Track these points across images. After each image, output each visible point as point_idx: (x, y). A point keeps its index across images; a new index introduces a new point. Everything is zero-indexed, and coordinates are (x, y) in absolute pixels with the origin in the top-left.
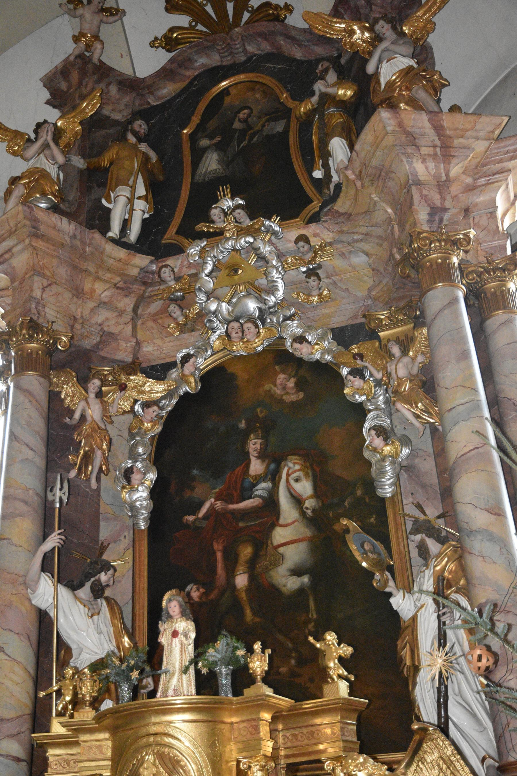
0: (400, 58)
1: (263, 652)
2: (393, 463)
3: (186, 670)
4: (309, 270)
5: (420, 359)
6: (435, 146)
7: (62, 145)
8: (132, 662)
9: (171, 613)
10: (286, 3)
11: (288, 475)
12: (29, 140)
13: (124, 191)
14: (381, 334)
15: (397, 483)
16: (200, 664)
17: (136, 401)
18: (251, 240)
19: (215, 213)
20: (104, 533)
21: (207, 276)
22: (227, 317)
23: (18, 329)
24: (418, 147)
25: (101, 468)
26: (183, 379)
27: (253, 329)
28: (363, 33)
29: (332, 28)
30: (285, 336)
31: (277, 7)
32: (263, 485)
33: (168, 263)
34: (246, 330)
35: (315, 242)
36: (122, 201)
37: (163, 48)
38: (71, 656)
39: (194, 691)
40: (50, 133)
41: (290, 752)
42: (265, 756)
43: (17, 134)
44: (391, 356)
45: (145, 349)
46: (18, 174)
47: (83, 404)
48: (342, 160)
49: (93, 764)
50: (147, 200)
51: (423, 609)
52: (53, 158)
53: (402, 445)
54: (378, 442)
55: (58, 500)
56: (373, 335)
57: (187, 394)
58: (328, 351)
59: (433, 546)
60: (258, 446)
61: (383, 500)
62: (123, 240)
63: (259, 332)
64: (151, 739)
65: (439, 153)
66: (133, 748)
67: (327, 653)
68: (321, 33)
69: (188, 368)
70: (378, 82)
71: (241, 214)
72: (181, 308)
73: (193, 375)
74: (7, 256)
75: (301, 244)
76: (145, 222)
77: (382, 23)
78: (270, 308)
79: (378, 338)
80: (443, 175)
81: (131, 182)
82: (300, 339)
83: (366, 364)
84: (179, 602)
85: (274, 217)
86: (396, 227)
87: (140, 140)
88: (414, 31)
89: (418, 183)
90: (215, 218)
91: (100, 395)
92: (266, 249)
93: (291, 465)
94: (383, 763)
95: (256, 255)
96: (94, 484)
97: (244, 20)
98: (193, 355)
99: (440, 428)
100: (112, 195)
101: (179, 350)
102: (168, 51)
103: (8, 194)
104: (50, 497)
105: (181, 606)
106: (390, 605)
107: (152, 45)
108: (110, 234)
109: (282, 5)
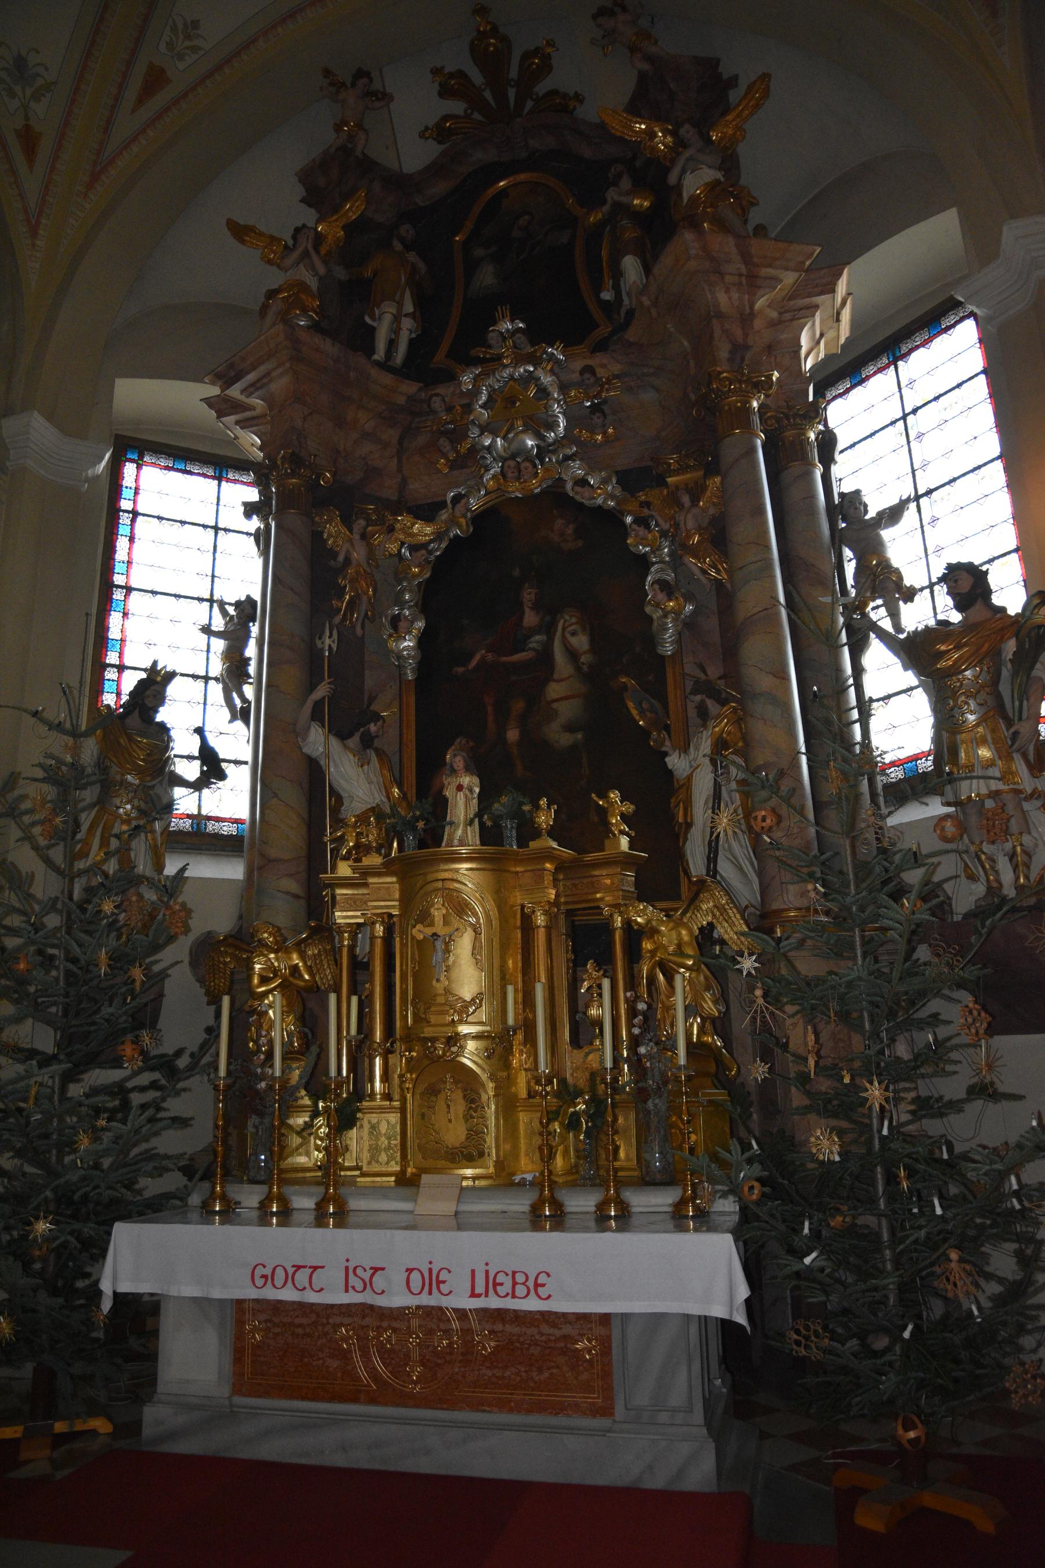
0: (706, 169)
1: (549, 807)
2: (674, 620)
3: (471, 823)
4: (593, 404)
5: (712, 511)
6: (741, 275)
7: (323, 252)
8: (418, 813)
9: (456, 767)
10: (576, 92)
11: (564, 629)
12: (286, 247)
13: (389, 310)
14: (669, 480)
15: (679, 641)
16: (486, 817)
17: (403, 544)
18: (532, 369)
19: (492, 337)
20: (370, 681)
21: (481, 407)
22: (503, 454)
23: (279, 463)
24: (722, 275)
25: (366, 614)
26: (453, 521)
27: (531, 469)
28: (664, 136)
29: (631, 129)
30: (564, 476)
31: (565, 96)
32: (538, 638)
33: (437, 391)
34: (522, 468)
35: (601, 372)
36: (388, 318)
37: (434, 139)
38: (342, 804)
39: (478, 842)
40: (310, 240)
41: (569, 899)
42: (549, 902)
43: (273, 239)
44: (681, 506)
45: (411, 487)
46: (275, 286)
47: (347, 546)
48: (634, 282)
49: (383, 903)
50: (414, 318)
51: (699, 770)
52: (313, 268)
53: (686, 601)
54: (661, 596)
55: (327, 648)
56: (661, 482)
57: (456, 536)
58: (612, 497)
59: (712, 706)
60: (533, 596)
61: (662, 658)
62: (389, 363)
63: (537, 473)
64: (440, 884)
65: (744, 282)
66: (422, 892)
67: (610, 809)
68: (618, 134)
69: (460, 508)
70: (680, 195)
71: (521, 339)
72: (451, 442)
73: (464, 516)
74: (265, 380)
75: (587, 376)
76: (412, 342)
77: (687, 126)
78: (550, 445)
79: (665, 484)
80: (747, 307)
81: (397, 297)
82: (582, 482)
83: (653, 513)
84: (464, 757)
85: (558, 343)
86: (692, 363)
87: (408, 248)
88: (721, 138)
89: (720, 315)
90: (492, 342)
91: (364, 536)
92: (546, 379)
93: (567, 617)
94: (661, 910)
95: (536, 386)
96: (359, 631)
97: (526, 110)
98: (465, 495)
99: (729, 586)
100: (377, 312)
101: (450, 489)
102: (440, 143)
103: (264, 309)
104: (318, 643)
105: (465, 761)
106: (665, 763)
107: (422, 135)
108: (376, 357)
109: (572, 94)
